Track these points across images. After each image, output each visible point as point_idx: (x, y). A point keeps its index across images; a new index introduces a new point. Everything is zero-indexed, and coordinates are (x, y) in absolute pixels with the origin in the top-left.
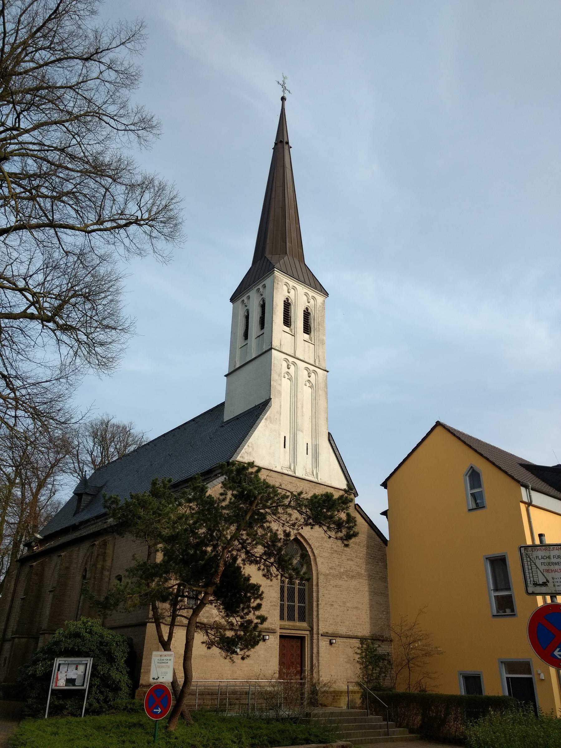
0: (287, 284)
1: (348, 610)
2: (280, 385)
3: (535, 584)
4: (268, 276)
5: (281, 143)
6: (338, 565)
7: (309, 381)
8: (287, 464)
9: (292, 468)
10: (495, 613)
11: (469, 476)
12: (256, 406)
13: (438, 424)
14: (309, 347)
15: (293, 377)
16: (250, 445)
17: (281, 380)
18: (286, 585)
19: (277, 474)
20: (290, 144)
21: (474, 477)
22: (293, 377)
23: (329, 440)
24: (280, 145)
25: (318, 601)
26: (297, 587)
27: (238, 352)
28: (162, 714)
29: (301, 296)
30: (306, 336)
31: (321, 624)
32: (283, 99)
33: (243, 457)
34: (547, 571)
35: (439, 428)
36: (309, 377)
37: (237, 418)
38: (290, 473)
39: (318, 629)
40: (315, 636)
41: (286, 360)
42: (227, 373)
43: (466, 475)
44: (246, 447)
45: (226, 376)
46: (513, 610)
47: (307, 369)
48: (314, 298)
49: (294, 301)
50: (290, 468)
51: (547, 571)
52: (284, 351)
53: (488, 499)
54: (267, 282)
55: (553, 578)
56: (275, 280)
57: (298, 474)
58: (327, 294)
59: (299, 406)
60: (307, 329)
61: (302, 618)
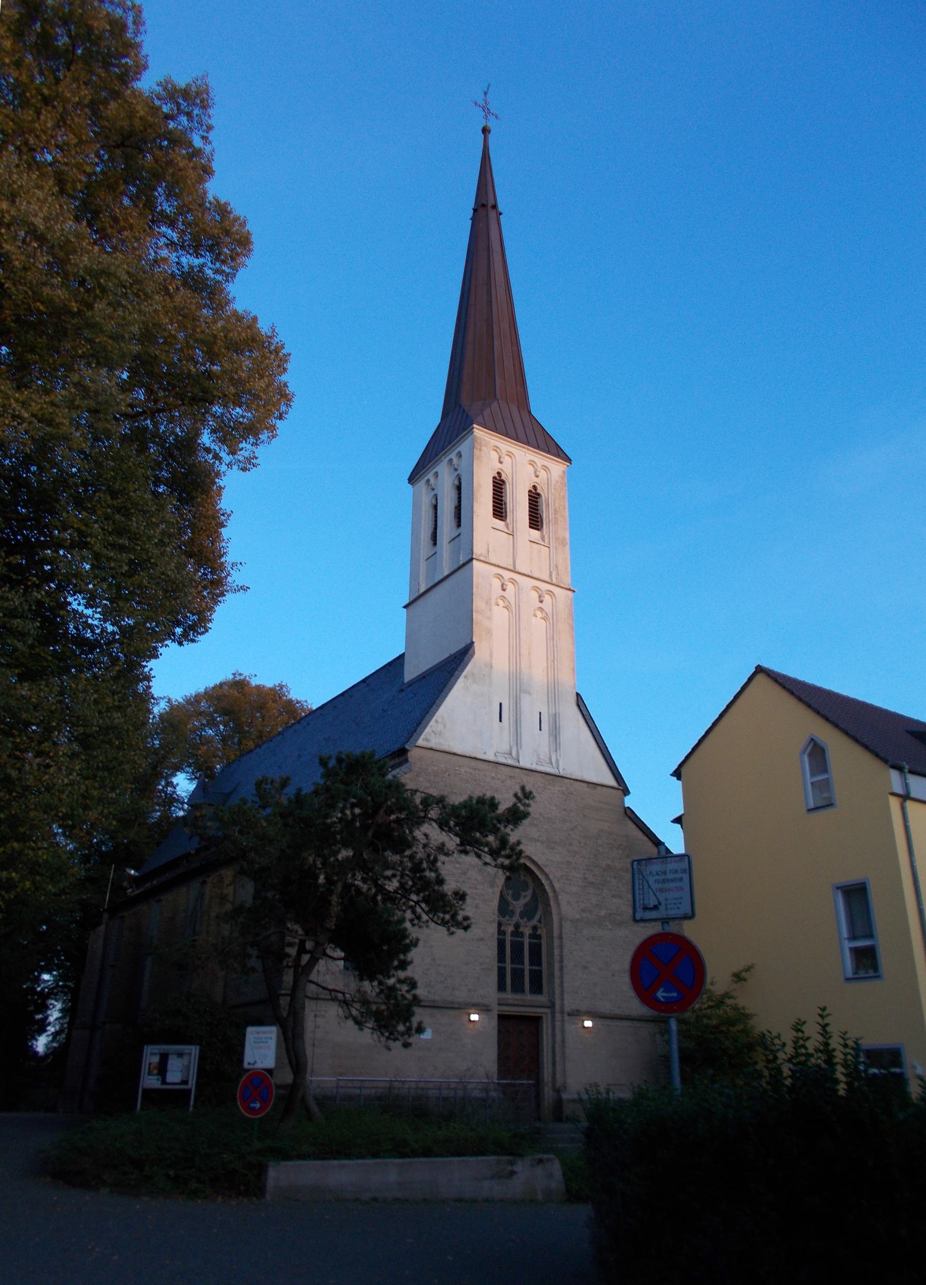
0: (496, 449)
1: (613, 975)
2: (489, 618)
3: (645, 908)
4: (463, 438)
5: (485, 208)
6: (597, 905)
7: (541, 609)
8: (505, 747)
9: (514, 754)
10: (850, 974)
11: (809, 755)
12: (451, 656)
13: (759, 670)
14: (539, 551)
15: (513, 603)
16: (440, 720)
17: (490, 610)
18: (508, 938)
19: (487, 764)
20: (500, 209)
21: (817, 753)
22: (513, 603)
23: (578, 705)
24: (481, 211)
25: (561, 961)
26: (526, 941)
27: (423, 566)
28: (261, 1109)
29: (523, 466)
30: (535, 534)
31: (566, 996)
32: (485, 131)
33: (427, 740)
34: (661, 890)
35: (760, 677)
36: (541, 602)
37: (423, 677)
38: (510, 762)
39: (562, 1005)
40: (558, 1016)
41: (499, 577)
42: (407, 602)
43: (804, 753)
44: (432, 723)
45: (405, 607)
46: (875, 968)
47: (536, 588)
48: (545, 468)
49: (510, 477)
50: (510, 754)
51: (661, 890)
52: (493, 562)
53: (839, 792)
54: (463, 447)
55: (666, 899)
56: (476, 445)
57: (524, 763)
58: (568, 459)
59: (524, 651)
60: (535, 521)
61: (537, 988)
